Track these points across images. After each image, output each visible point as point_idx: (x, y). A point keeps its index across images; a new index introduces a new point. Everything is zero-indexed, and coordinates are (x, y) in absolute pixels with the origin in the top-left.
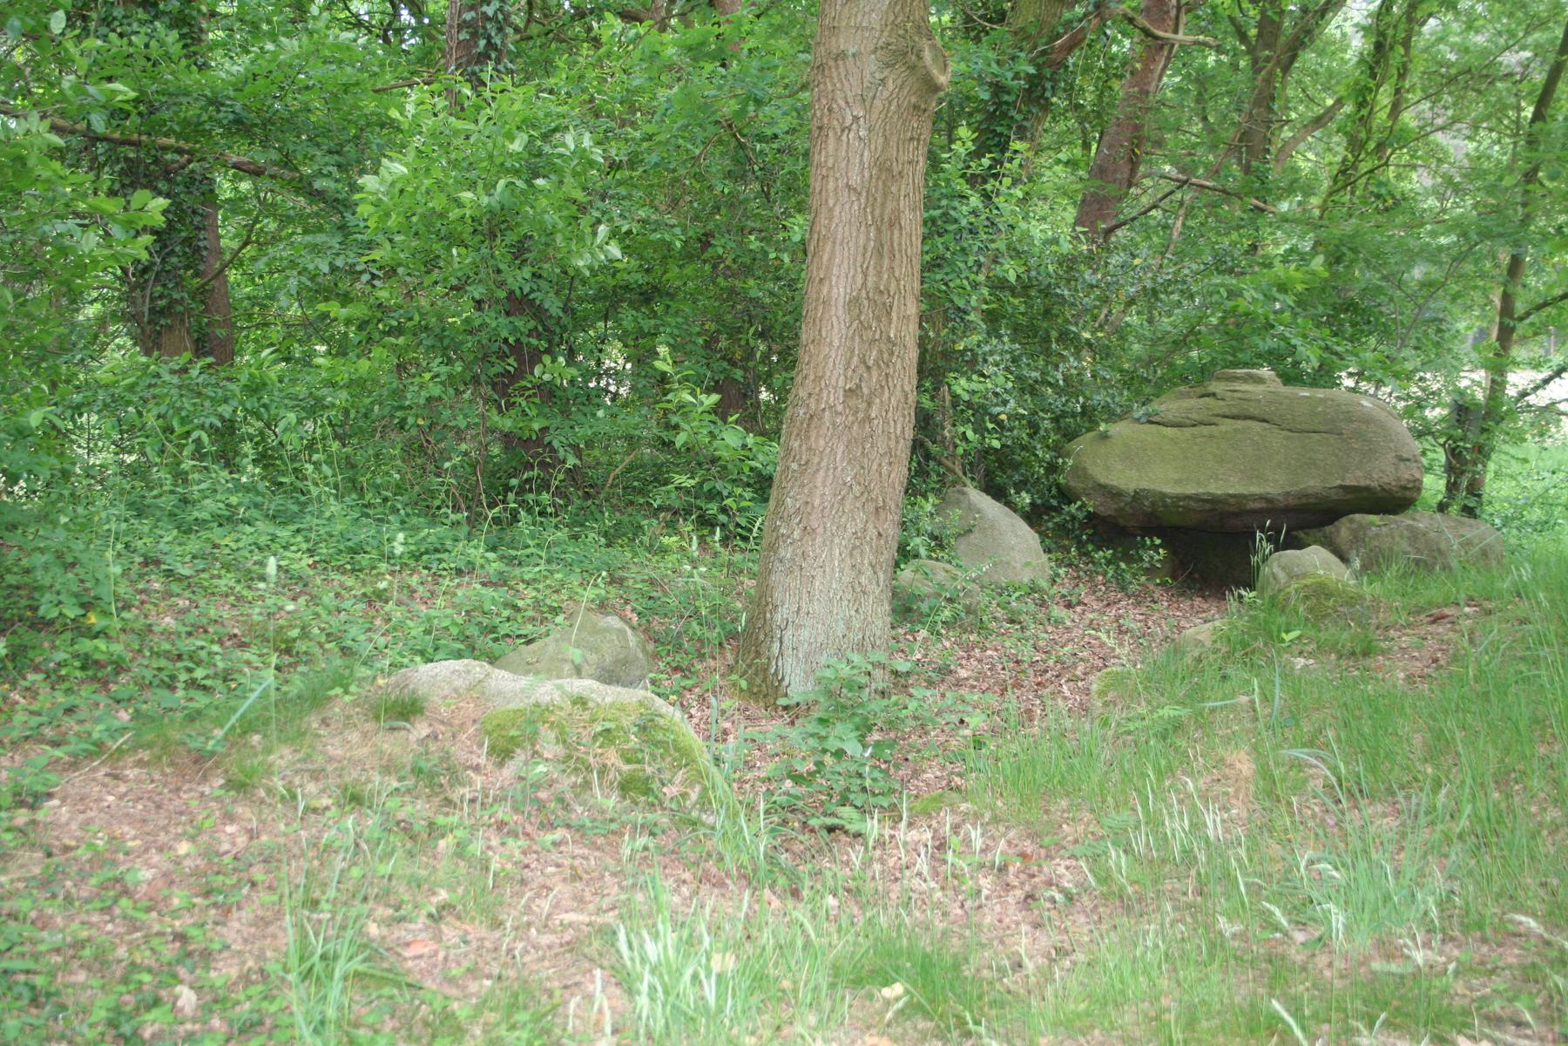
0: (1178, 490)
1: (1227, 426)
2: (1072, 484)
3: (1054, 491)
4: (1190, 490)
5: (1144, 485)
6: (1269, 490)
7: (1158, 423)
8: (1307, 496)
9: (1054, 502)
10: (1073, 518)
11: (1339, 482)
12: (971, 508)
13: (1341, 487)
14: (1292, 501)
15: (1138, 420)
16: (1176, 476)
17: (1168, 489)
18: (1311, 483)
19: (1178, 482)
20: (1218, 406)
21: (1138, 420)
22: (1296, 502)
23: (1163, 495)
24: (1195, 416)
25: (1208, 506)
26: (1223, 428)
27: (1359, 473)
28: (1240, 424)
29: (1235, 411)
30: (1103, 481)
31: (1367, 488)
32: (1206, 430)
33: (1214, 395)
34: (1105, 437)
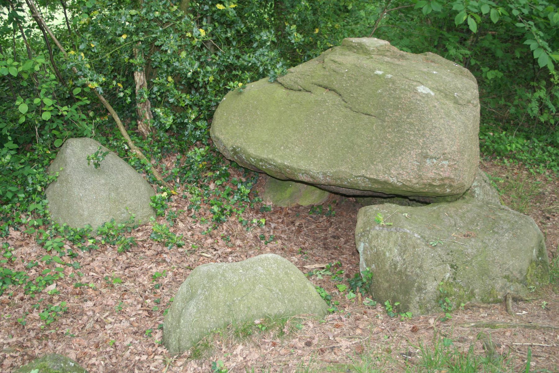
18: (343, 169)
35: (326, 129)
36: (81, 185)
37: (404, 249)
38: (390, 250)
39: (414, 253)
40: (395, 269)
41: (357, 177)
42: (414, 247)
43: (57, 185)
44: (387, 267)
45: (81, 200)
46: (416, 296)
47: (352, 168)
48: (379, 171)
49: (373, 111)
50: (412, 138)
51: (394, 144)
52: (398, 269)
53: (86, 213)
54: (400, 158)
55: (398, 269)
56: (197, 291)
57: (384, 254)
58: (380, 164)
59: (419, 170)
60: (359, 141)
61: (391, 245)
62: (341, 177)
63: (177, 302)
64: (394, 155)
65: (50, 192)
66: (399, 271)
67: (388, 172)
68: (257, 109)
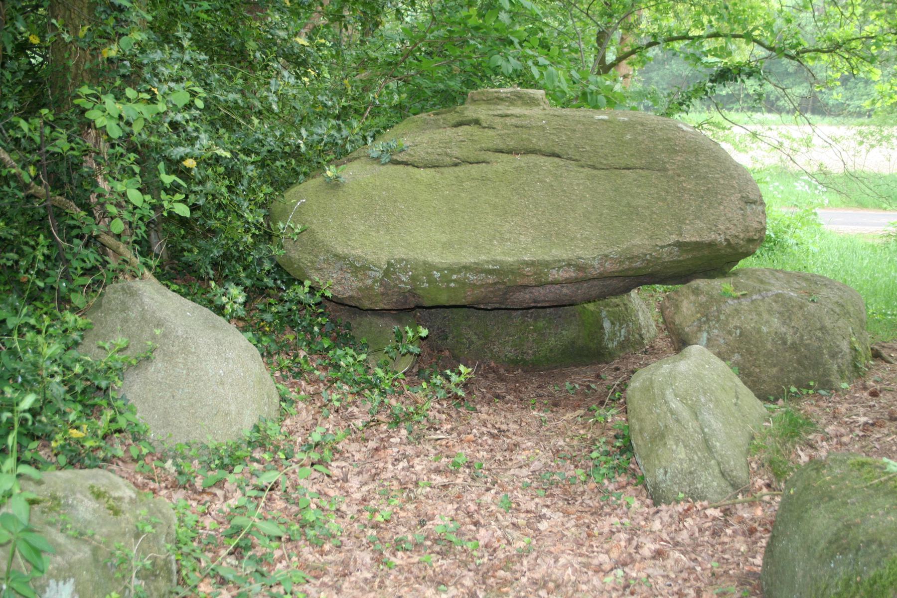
0: (450, 259)
1: (503, 163)
4: (468, 258)
5: (400, 253)
6: (580, 253)
7: (406, 164)
8: (631, 259)
11: (674, 238)
12: (148, 320)
13: (678, 244)
15: (377, 159)
16: (444, 238)
17: (435, 258)
18: (637, 241)
19: (448, 246)
20: (489, 138)
21: (377, 159)
22: (616, 267)
23: (429, 268)
24: (456, 152)
25: (491, 279)
26: (499, 167)
27: (699, 224)
28: (520, 160)
29: (512, 144)
30: (340, 250)
31: (711, 245)
32: (474, 170)
33: (477, 122)
34: (335, 184)
35: (567, 199)
36: (218, 354)
37: (787, 314)
38: (767, 322)
39: (803, 315)
40: (785, 343)
41: (662, 247)
42: (801, 308)
43: (157, 369)
44: (769, 346)
45: (222, 383)
46: (832, 364)
47: (651, 237)
48: (702, 229)
49: (634, 161)
50: (722, 181)
51: (702, 193)
52: (789, 342)
53: (233, 408)
54: (722, 207)
55: (789, 342)
56: (699, 400)
57: (759, 331)
58: (698, 222)
59: (744, 220)
60: (642, 202)
61: (765, 316)
62: (636, 254)
63: (688, 421)
64: (711, 205)
65: (135, 388)
66: (792, 344)
67: (714, 228)
68: (395, 201)
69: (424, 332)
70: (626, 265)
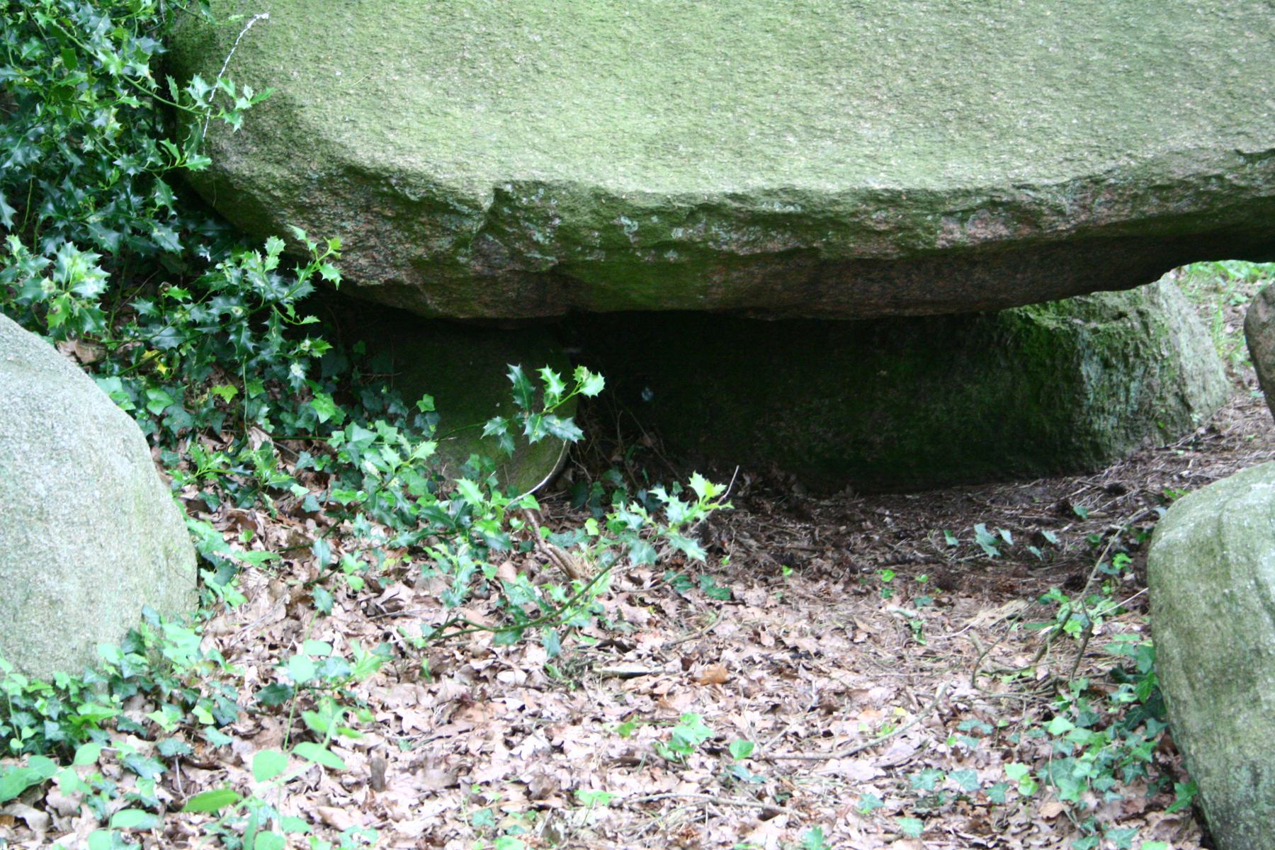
2: (239, 165)
3: (162, 196)
6: (1027, 172)
9: (168, 239)
10: (259, 310)
14: (1103, 212)
16: (650, 127)
18: (1184, 139)
22: (1125, 213)
23: (608, 202)
25: (777, 243)
30: (366, 154)
69: (593, 384)
70: (1152, 207)
